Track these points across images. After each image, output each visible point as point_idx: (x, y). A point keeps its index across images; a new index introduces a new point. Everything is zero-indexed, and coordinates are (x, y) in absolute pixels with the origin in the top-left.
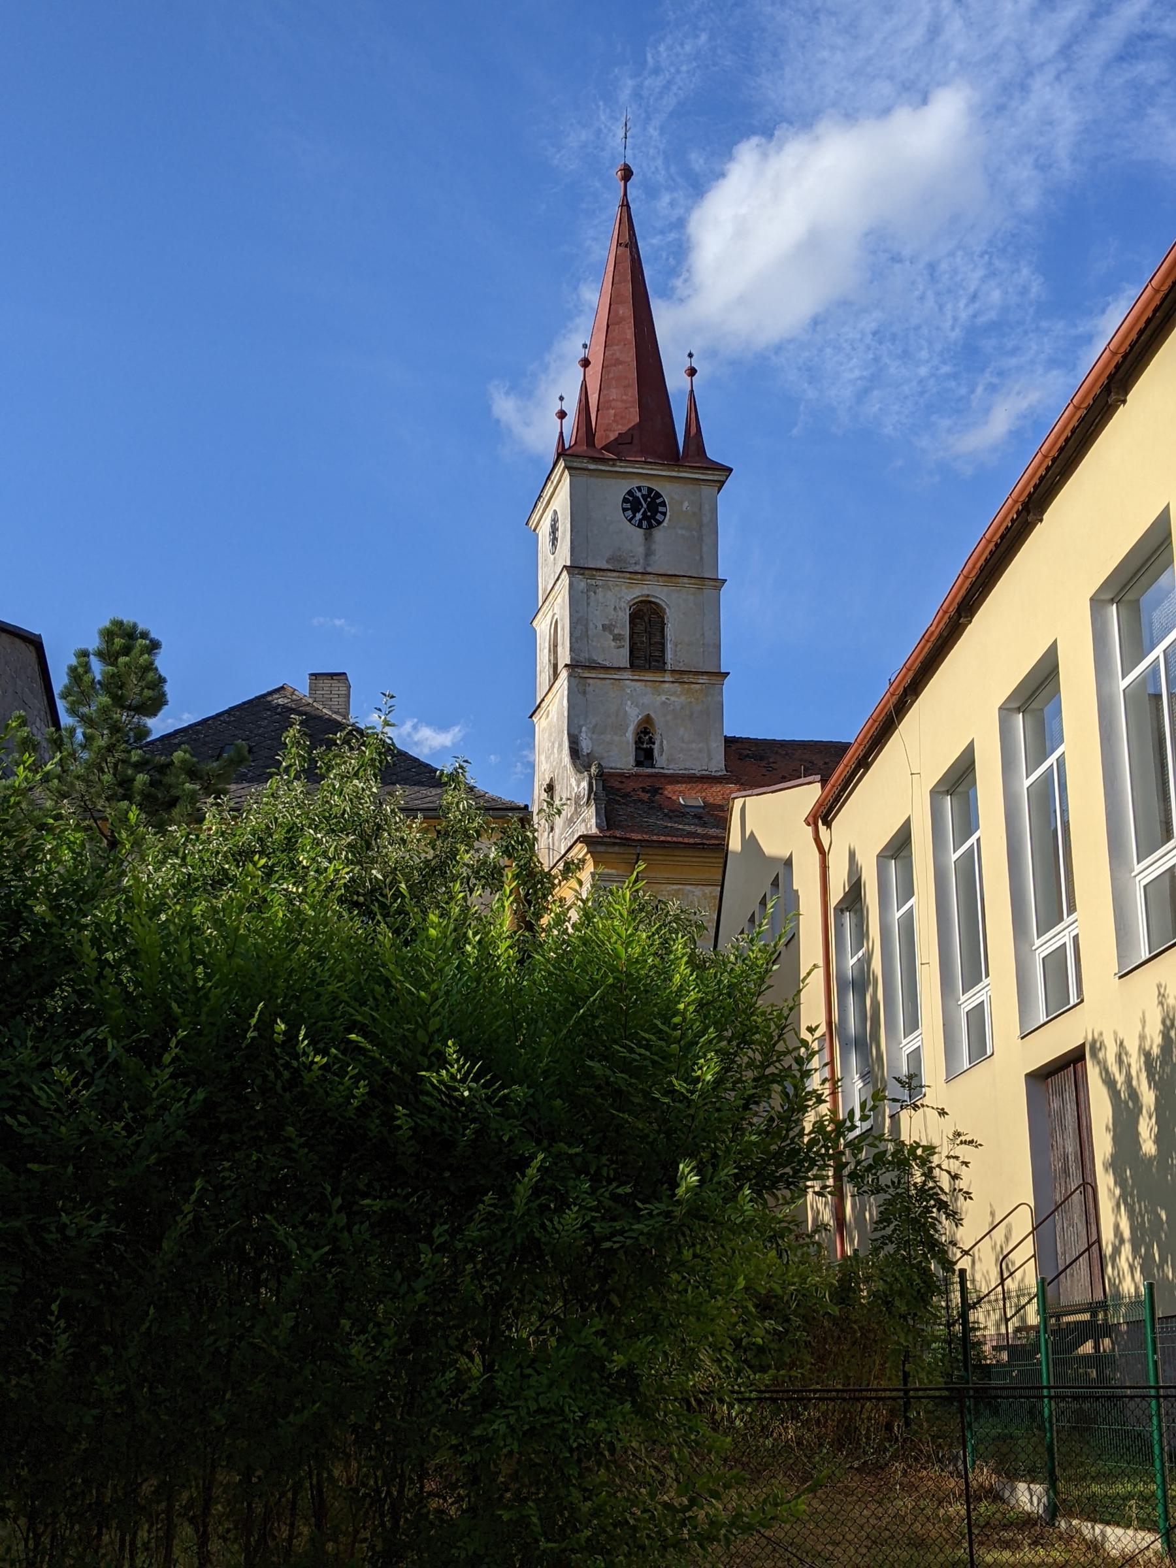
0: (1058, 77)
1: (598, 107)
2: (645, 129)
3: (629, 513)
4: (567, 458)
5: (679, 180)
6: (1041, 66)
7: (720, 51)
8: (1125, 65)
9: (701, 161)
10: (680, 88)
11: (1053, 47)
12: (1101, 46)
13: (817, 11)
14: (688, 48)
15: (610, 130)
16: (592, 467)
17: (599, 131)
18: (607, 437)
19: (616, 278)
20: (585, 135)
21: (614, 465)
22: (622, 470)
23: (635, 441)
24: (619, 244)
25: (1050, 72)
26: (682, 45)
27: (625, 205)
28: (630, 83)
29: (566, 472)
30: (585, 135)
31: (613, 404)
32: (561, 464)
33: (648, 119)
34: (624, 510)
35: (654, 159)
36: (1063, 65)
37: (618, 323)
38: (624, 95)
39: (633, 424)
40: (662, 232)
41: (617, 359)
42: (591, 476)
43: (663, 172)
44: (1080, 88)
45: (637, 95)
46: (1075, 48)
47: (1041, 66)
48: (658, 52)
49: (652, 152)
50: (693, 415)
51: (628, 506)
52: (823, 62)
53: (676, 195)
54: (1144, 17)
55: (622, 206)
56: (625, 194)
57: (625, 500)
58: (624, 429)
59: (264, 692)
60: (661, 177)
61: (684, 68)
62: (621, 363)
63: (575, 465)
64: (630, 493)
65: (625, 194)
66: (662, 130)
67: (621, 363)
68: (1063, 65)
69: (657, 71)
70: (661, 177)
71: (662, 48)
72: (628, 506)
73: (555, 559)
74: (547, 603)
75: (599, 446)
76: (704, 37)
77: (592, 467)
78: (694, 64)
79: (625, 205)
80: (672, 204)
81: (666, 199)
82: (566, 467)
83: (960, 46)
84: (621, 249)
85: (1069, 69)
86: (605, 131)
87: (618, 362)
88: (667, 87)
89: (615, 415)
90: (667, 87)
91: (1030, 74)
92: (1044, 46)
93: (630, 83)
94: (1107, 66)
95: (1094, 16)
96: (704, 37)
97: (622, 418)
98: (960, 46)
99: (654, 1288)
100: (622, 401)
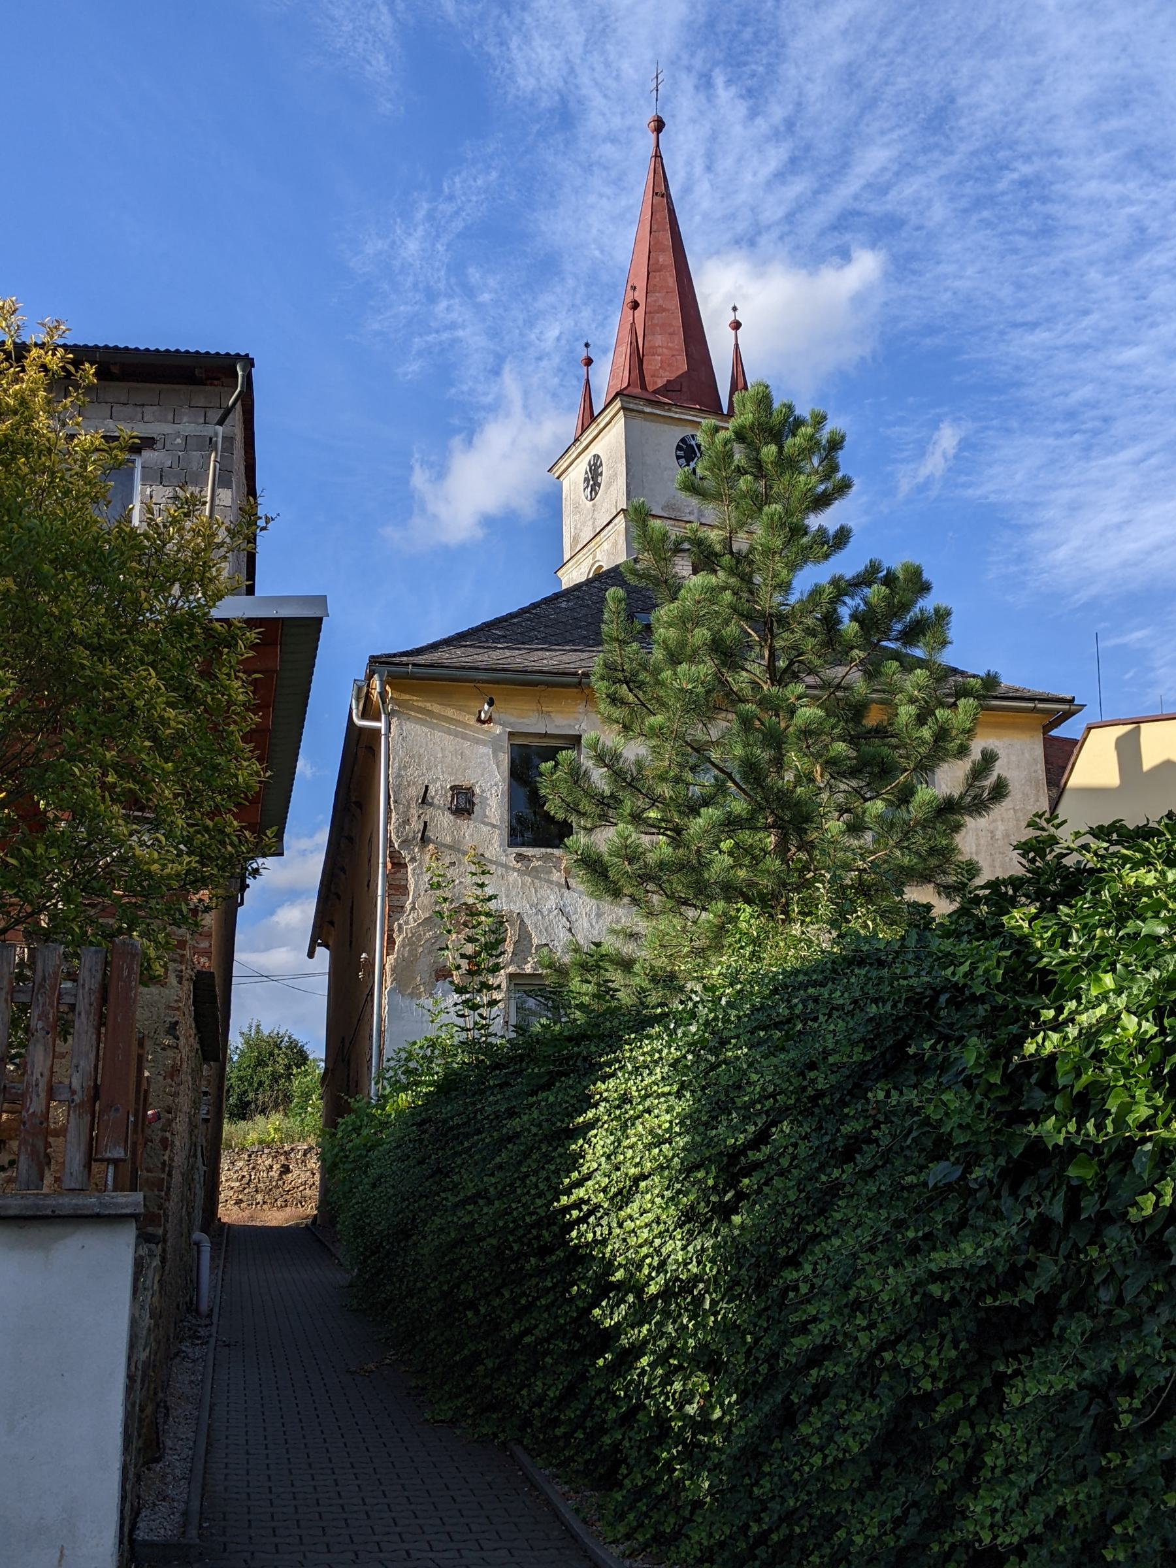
0: (781, 238)
1: (395, 223)
2: (433, 245)
3: (683, 461)
4: (625, 398)
5: (457, 289)
6: (768, 228)
7: (507, 188)
8: (836, 234)
9: (478, 275)
10: (468, 215)
11: (780, 213)
12: (819, 217)
13: (591, 165)
14: (479, 182)
15: (403, 242)
16: (648, 410)
17: (394, 242)
18: (655, 383)
19: (655, 227)
20: (381, 245)
21: (669, 411)
22: (677, 416)
23: (684, 389)
24: (655, 194)
25: (775, 233)
26: (475, 180)
27: (658, 156)
28: (426, 206)
29: (622, 413)
30: (381, 245)
31: (660, 350)
32: (617, 404)
33: (438, 236)
34: (678, 457)
35: (438, 270)
36: (787, 228)
37: (660, 271)
38: (420, 215)
39: (681, 372)
40: (437, 332)
41: (660, 306)
42: (646, 420)
43: (444, 282)
44: (798, 247)
45: (430, 217)
46: (798, 216)
47: (768, 228)
48: (454, 183)
49: (437, 264)
50: (740, 369)
51: (682, 454)
52: (592, 207)
53: (452, 302)
54: (856, 197)
55: (656, 156)
56: (658, 146)
57: (679, 448)
58: (673, 377)
59: (424, 644)
60: (442, 286)
61: (474, 198)
62: (664, 310)
63: (631, 406)
64: (683, 440)
65: (658, 146)
66: (449, 247)
67: (664, 310)
68: (787, 228)
69: (451, 198)
70: (442, 286)
71: (457, 179)
72: (682, 454)
73: (594, 505)
74: (586, 550)
75: (650, 389)
76: (494, 175)
77: (648, 410)
78: (483, 196)
79: (658, 156)
80: (448, 309)
81: (443, 304)
82: (623, 408)
83: (705, 205)
84: (657, 199)
85: (790, 232)
86: (398, 243)
87: (662, 309)
88: (457, 213)
89: (662, 362)
90: (457, 213)
91: (759, 233)
92: (773, 211)
93: (426, 206)
94: (822, 234)
95: (816, 192)
96: (494, 175)
97: (669, 365)
98: (705, 205)
99: (747, 1175)
100: (667, 348)
